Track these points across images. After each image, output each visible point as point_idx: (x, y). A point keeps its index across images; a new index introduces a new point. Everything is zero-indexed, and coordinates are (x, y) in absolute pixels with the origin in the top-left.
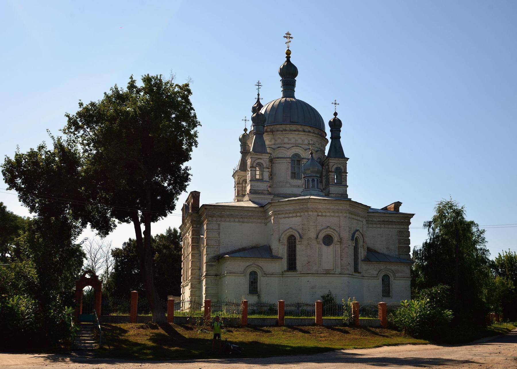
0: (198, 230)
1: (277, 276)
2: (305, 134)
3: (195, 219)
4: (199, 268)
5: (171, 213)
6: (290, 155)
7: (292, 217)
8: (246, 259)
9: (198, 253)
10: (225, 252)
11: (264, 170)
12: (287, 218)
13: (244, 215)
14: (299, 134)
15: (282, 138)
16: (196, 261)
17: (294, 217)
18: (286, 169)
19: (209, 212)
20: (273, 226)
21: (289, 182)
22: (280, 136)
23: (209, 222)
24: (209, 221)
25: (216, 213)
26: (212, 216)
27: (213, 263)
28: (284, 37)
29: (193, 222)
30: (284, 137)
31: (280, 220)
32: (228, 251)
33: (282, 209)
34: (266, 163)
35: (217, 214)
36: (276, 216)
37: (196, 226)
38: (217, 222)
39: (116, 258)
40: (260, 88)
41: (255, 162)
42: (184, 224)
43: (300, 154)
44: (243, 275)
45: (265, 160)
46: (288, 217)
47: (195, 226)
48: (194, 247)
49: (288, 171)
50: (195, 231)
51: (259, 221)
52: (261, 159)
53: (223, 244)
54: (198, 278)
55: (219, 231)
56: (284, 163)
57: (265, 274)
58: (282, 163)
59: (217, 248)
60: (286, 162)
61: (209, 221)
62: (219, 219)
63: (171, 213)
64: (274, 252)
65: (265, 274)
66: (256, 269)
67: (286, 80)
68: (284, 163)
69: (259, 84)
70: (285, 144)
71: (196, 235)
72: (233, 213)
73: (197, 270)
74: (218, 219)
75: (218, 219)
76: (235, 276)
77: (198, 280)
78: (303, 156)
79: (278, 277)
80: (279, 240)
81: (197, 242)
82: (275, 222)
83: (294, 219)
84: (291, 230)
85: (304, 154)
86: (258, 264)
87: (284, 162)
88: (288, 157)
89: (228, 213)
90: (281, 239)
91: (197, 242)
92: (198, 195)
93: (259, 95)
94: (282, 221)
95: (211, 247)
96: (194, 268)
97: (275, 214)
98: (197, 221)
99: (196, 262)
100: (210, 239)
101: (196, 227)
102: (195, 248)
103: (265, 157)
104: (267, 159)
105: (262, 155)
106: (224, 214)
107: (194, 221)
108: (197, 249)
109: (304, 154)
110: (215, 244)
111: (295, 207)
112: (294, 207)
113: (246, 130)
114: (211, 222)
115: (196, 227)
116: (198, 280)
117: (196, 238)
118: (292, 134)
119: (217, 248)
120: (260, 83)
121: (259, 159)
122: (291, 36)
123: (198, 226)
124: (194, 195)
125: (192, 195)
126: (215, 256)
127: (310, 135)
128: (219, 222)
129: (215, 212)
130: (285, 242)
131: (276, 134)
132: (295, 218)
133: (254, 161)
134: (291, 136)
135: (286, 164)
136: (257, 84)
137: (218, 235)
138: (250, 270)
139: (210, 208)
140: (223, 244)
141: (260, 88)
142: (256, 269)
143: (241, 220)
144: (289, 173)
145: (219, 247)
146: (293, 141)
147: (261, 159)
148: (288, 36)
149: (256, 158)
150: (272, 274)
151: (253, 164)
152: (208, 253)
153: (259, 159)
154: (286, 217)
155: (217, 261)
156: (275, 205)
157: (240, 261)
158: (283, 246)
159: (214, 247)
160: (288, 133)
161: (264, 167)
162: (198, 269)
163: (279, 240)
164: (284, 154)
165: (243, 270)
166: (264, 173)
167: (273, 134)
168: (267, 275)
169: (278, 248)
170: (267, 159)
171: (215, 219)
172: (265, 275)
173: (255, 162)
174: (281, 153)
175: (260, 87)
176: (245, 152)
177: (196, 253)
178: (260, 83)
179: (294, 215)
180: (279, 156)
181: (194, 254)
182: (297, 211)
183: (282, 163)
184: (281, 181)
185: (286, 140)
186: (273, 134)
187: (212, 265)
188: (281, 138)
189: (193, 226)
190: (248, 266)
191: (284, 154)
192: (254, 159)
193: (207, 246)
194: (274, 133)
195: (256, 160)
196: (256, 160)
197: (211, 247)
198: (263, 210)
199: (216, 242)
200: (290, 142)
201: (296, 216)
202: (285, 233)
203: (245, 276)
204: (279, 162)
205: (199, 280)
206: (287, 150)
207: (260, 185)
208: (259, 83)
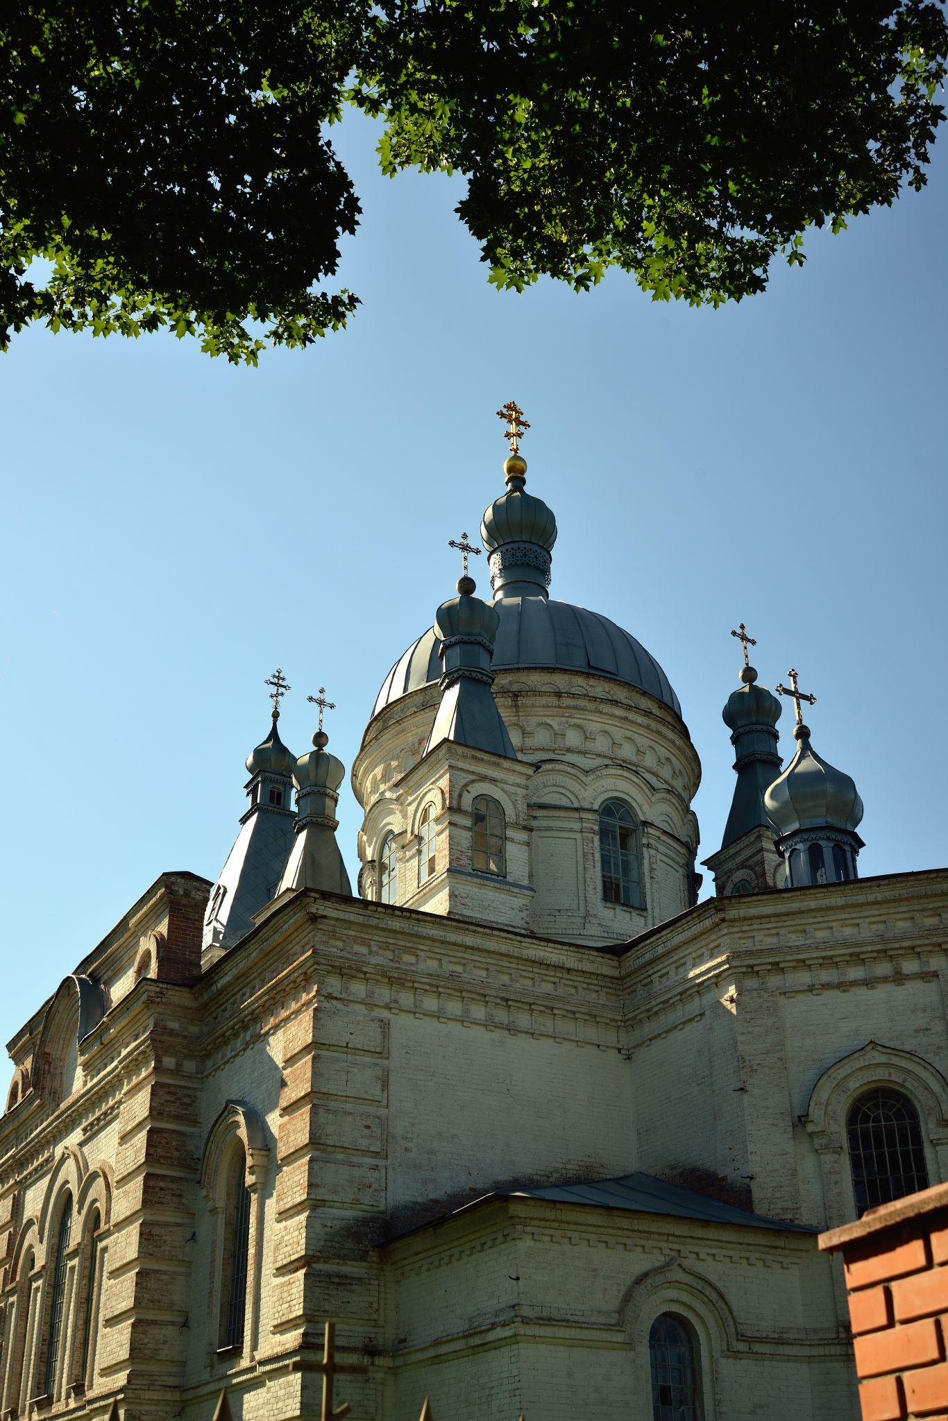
0: (188, 1088)
1: (806, 1351)
2: (648, 727)
3: (174, 1025)
4: (181, 1319)
5: (248, 795)
6: (595, 798)
7: (868, 983)
8: (637, 1224)
9: (178, 1225)
10: (420, 1200)
11: (510, 833)
12: (836, 993)
13: (518, 985)
14: (626, 719)
15: (556, 727)
16: (165, 1273)
17: (885, 979)
18: (580, 859)
19: (332, 942)
20: (740, 1038)
21: (595, 916)
22: (545, 719)
23: (326, 1004)
24: (330, 997)
25: (370, 953)
26: (346, 971)
27: (353, 1269)
28: (498, 413)
29: (165, 1038)
30: (567, 722)
31: (782, 1001)
32: (432, 1196)
33: (795, 940)
34: (515, 806)
35: (374, 960)
36: (751, 983)
37: (179, 1065)
38: (371, 1006)
39: (362, 96)
40: (282, 694)
41: (469, 788)
42: (47, 1091)
43: (634, 805)
44: (619, 1338)
45: (509, 788)
46: (842, 986)
47: (169, 1062)
48: (162, 1184)
49: (589, 864)
50: (169, 1093)
51: (590, 1032)
52: (493, 781)
53: (411, 1145)
54: (172, 1381)
55: (386, 1062)
56: (571, 830)
57: (741, 1337)
58: (562, 830)
59: (375, 1168)
60: (577, 826)
61: (330, 997)
62: (384, 994)
63: (248, 795)
64: (766, 1200)
65: (741, 1337)
66: (686, 1298)
67: (507, 550)
68: (571, 830)
69: (281, 682)
70: (569, 750)
71: (177, 1118)
72: (459, 969)
73: (170, 1332)
74: (377, 991)
75: (377, 991)
76: (572, 1343)
77: (168, 1396)
78: (643, 813)
79: (810, 1359)
80: (801, 1121)
81: (176, 1154)
82: (748, 1016)
83: (880, 994)
84: (877, 1057)
85: (646, 807)
86: (699, 1267)
87: (568, 825)
88: (586, 805)
89: (432, 965)
90: (815, 1113)
91: (176, 1154)
92: (199, 896)
93: (276, 715)
94: (797, 1010)
95: (340, 1157)
96: (150, 1315)
97: (752, 971)
98: (185, 1037)
99: (165, 1277)
100: (333, 1105)
101: (177, 1072)
102: (162, 1189)
103: (512, 778)
104: (518, 785)
105: (498, 765)
106: (411, 964)
107: (171, 1032)
108: (175, 1199)
109: (646, 807)
110: (363, 1143)
111: (881, 927)
112: (874, 927)
113: (323, 740)
114: (339, 1005)
115: (177, 1072)
116: (168, 1396)
117: (174, 1131)
118: (601, 713)
119: (375, 1168)
120: (283, 679)
121: (484, 778)
122: (522, 418)
123: (190, 1066)
124: (181, 892)
125: (170, 891)
126: (364, 1222)
127: (666, 738)
128: (385, 1014)
129: (364, 950)
130: (839, 1130)
131: (533, 706)
132: (890, 987)
133: (466, 785)
134: (594, 724)
135: (578, 836)
136: (273, 680)
137: (379, 1087)
138: (651, 1308)
139: (341, 915)
140: (406, 1149)
141: (282, 694)
142: (686, 1298)
143: (501, 1015)
144: (596, 875)
145: (381, 1163)
146: (602, 745)
147: (493, 781)
148: (511, 413)
149: (473, 773)
150: (780, 1342)
151: (460, 796)
152: (321, 1194)
153: (484, 778)
154: (826, 986)
155: (374, 1256)
156: (745, 919)
157: (593, 1237)
158: (829, 1158)
159: (355, 1159)
160: (583, 709)
161: (507, 819)
162: (172, 1323)
163: (801, 1121)
164: (567, 793)
165: (614, 1303)
166: (507, 846)
167: (516, 706)
168: (757, 1347)
169: (794, 1173)
170: (518, 785)
171: (358, 988)
172: (742, 1346)
173: (469, 788)
174: (555, 789)
175: (282, 690)
176: (320, 820)
177: (167, 1225)
178: (283, 679)
179: (883, 969)
180: (547, 800)
181: (156, 1230)
182: (905, 944)
183: (562, 830)
184: (559, 911)
185: (573, 738)
186: (516, 706)
187: (342, 1281)
188: (552, 727)
189: (158, 1061)
190: (646, 1275)
191: (567, 793)
192: (463, 775)
193: (317, 1153)
194: (521, 701)
195: (473, 781)
196: (473, 781)
197: (340, 1157)
198: (615, 973)
199: (367, 1132)
200: (589, 746)
201: (899, 978)
202: (843, 1071)
203: (629, 1345)
204: (545, 823)
205: (177, 1396)
206: (584, 779)
207: (493, 901)
208: (278, 678)
